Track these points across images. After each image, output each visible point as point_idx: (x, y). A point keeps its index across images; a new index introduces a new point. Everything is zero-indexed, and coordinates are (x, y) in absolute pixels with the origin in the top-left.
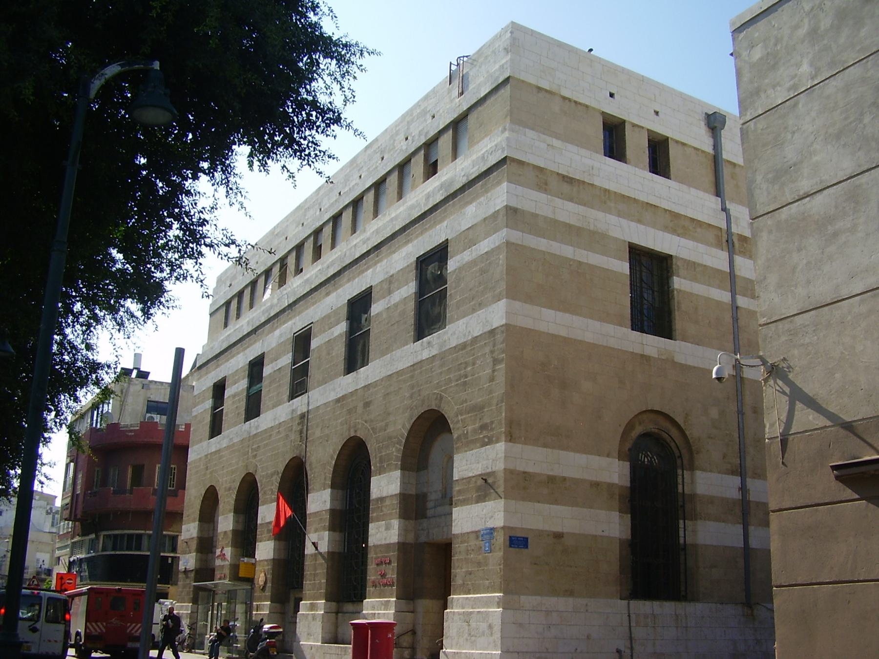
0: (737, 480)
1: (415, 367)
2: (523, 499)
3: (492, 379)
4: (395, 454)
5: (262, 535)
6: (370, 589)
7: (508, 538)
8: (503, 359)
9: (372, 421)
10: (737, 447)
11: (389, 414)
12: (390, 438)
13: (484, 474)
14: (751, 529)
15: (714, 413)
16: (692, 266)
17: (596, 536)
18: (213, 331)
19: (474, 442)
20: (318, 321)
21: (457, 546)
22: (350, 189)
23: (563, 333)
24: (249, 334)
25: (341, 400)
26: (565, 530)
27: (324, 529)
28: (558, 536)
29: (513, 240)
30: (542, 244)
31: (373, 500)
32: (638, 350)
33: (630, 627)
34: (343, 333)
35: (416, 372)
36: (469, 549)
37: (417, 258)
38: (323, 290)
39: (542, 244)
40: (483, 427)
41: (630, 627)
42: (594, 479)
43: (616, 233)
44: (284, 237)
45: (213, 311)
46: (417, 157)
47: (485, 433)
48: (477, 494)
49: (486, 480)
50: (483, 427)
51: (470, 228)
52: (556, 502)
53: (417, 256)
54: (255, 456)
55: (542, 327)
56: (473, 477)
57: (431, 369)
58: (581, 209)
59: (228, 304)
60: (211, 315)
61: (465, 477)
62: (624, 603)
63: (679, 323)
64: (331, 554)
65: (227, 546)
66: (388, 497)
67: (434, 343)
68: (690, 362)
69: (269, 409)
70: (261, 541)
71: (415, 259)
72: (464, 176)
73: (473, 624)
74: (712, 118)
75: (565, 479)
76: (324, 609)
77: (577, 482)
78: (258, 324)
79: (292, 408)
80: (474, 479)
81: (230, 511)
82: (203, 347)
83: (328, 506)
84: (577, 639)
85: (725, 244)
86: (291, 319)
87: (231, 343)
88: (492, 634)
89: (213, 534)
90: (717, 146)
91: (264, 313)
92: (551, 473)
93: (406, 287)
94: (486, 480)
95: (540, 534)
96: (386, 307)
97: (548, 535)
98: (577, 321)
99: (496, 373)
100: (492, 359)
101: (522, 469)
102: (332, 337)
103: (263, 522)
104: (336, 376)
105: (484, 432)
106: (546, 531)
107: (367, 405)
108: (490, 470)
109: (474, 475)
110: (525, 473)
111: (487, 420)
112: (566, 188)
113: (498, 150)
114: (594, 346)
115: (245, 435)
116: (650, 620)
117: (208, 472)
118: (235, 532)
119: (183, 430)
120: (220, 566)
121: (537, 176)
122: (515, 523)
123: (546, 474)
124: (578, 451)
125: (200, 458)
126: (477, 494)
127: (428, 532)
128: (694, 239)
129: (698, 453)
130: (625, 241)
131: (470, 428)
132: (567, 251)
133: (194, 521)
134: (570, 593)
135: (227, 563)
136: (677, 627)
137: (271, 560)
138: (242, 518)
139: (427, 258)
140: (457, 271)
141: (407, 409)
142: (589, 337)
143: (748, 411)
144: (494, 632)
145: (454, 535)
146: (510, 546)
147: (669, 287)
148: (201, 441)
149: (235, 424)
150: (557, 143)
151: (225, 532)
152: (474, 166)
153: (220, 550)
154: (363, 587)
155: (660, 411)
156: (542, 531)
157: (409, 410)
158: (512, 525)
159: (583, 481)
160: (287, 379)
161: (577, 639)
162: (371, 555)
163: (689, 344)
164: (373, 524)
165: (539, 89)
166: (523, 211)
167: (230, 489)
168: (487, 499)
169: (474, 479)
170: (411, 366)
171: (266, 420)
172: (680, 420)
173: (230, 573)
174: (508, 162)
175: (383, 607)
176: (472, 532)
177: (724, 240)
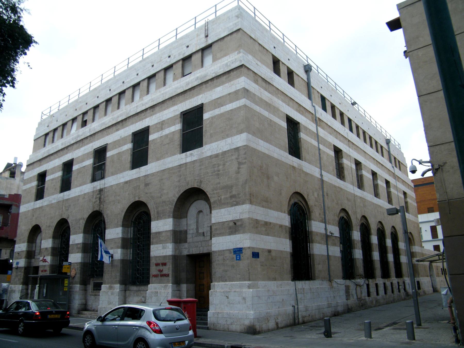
0: (323, 225)
1: (181, 166)
2: (257, 233)
3: (238, 172)
4: (168, 210)
5: (72, 250)
6: (152, 279)
7: (252, 253)
8: (245, 163)
9: (151, 193)
10: (323, 210)
11: (163, 190)
12: (165, 202)
13: (234, 220)
14: (329, 246)
15: (316, 195)
16: (306, 128)
17: (282, 251)
18: (35, 149)
19: (224, 204)
20: (111, 143)
21: (216, 257)
22: (131, 80)
23: (267, 152)
24: (62, 150)
25: (128, 182)
26: (272, 249)
27: (118, 248)
28: (270, 251)
29: (247, 105)
30: (257, 108)
31: (153, 233)
32: (291, 164)
33: (296, 294)
34: (129, 149)
35: (182, 169)
36: (225, 258)
37: (181, 112)
38: (114, 128)
39: (257, 108)
40: (232, 197)
41: (296, 294)
42: (281, 224)
43: (282, 109)
44: (85, 103)
45: (36, 138)
46: (177, 65)
47: (234, 199)
48: (229, 230)
49: (235, 224)
50: (232, 197)
51: (219, 98)
52: (268, 235)
53: (181, 111)
54: (67, 210)
55: (259, 148)
56: (226, 222)
57: (193, 167)
58: (269, 95)
59: (47, 135)
60: (34, 140)
61: (220, 222)
62: (293, 283)
63: (304, 153)
64: (123, 261)
65: (48, 255)
66: (164, 231)
67: (195, 154)
68: (308, 171)
69: (77, 186)
70: (72, 253)
71: (180, 113)
72: (214, 73)
73: (231, 298)
74: (307, 67)
75: (271, 223)
76: (119, 289)
77: (275, 225)
78: (69, 144)
79: (93, 186)
80: (227, 223)
81: (50, 238)
82: (30, 156)
83: (120, 236)
84: (279, 302)
85: (315, 121)
86: (92, 142)
87: (50, 154)
88: (245, 303)
89: (35, 249)
90: (308, 78)
91: (73, 139)
92: (266, 220)
93: (174, 126)
94: (235, 224)
95: (263, 250)
96: (160, 136)
97: (266, 251)
98: (272, 148)
99: (240, 169)
100: (237, 162)
101: (255, 218)
102: (121, 151)
103: (73, 243)
104: (124, 170)
105: (233, 199)
106: (265, 249)
107: (147, 185)
108: (238, 218)
109: (226, 221)
110: (256, 220)
111: (234, 193)
112: (264, 84)
113: (237, 61)
114: (277, 160)
115: (61, 199)
116: (302, 290)
117: (34, 218)
118: (53, 249)
119: (8, 197)
120: (42, 265)
121: (254, 77)
122: (254, 246)
123: (264, 221)
124: (274, 210)
125: (28, 211)
126: (229, 230)
127: (189, 250)
128: (305, 117)
129: (312, 212)
130: (285, 113)
131: (223, 197)
132: (266, 113)
133: (24, 242)
134: (275, 279)
135: (46, 264)
136: (311, 293)
137: (79, 263)
138: (58, 241)
139: (188, 113)
140: (210, 119)
141: (176, 187)
142: (275, 156)
143: (325, 194)
144: (246, 301)
145: (213, 251)
146: (253, 257)
147: (298, 137)
148: (29, 202)
149: (53, 194)
150: (259, 63)
151: (46, 249)
152: (220, 69)
153: (43, 257)
154: (149, 278)
155: (299, 193)
156: (264, 249)
157: (177, 188)
158: (253, 247)
159: (277, 224)
160: (90, 171)
161: (279, 302)
162: (153, 262)
163: (307, 164)
164: (153, 246)
165: (251, 37)
166: (250, 91)
167: (49, 226)
168: (237, 233)
169: (227, 223)
170: (178, 166)
171: (74, 192)
172: (306, 197)
173: (50, 270)
174: (244, 67)
175: (163, 288)
176: (227, 250)
177: (314, 119)
